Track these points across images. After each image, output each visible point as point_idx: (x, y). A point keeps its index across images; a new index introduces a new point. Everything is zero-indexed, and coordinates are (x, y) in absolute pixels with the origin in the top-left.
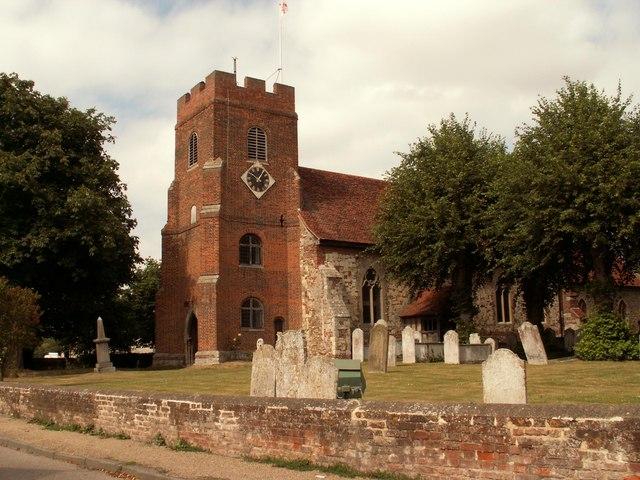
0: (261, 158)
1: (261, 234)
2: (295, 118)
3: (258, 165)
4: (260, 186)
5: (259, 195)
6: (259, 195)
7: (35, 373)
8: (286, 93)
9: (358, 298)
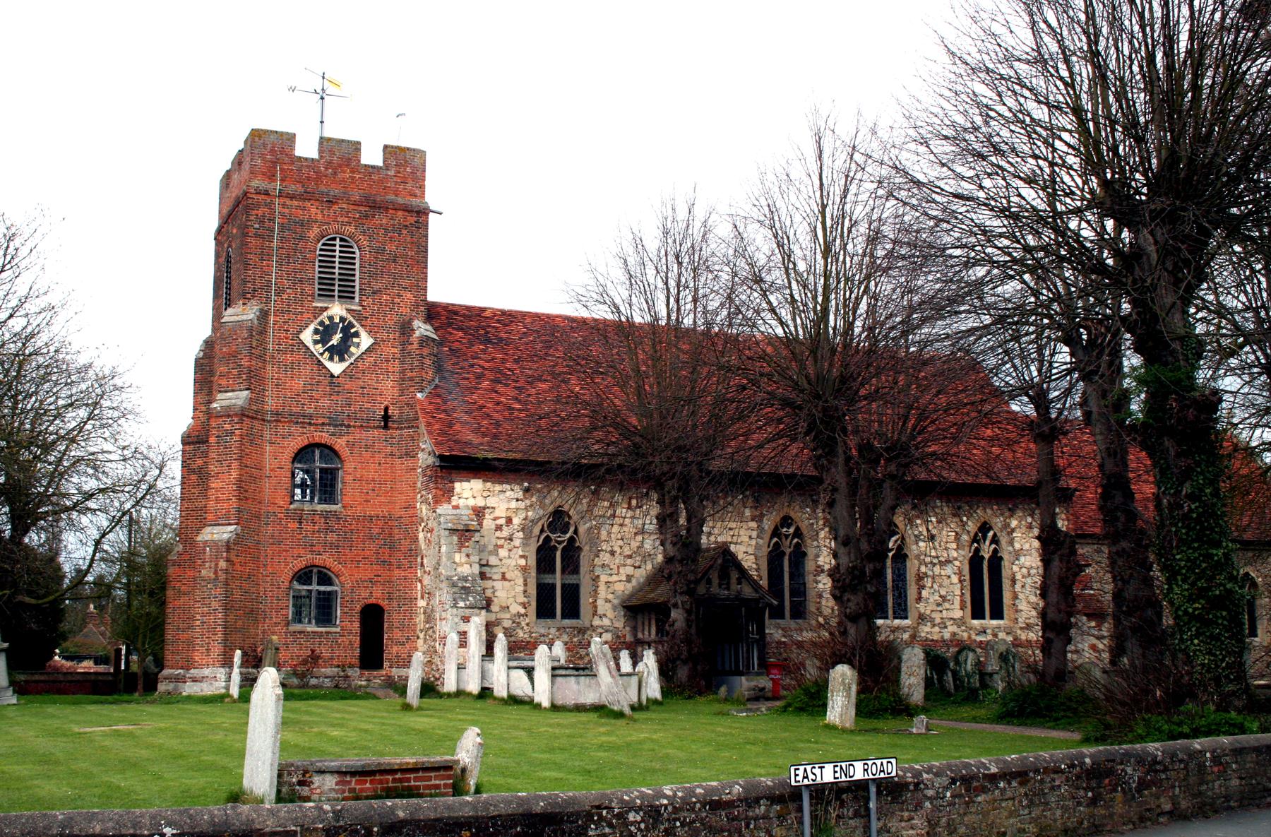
0: (346, 295)
1: (340, 444)
2: (421, 214)
3: (337, 310)
4: (339, 352)
5: (336, 368)
6: (336, 368)
7: (46, 697)
8: (359, 143)
9: (524, 569)
